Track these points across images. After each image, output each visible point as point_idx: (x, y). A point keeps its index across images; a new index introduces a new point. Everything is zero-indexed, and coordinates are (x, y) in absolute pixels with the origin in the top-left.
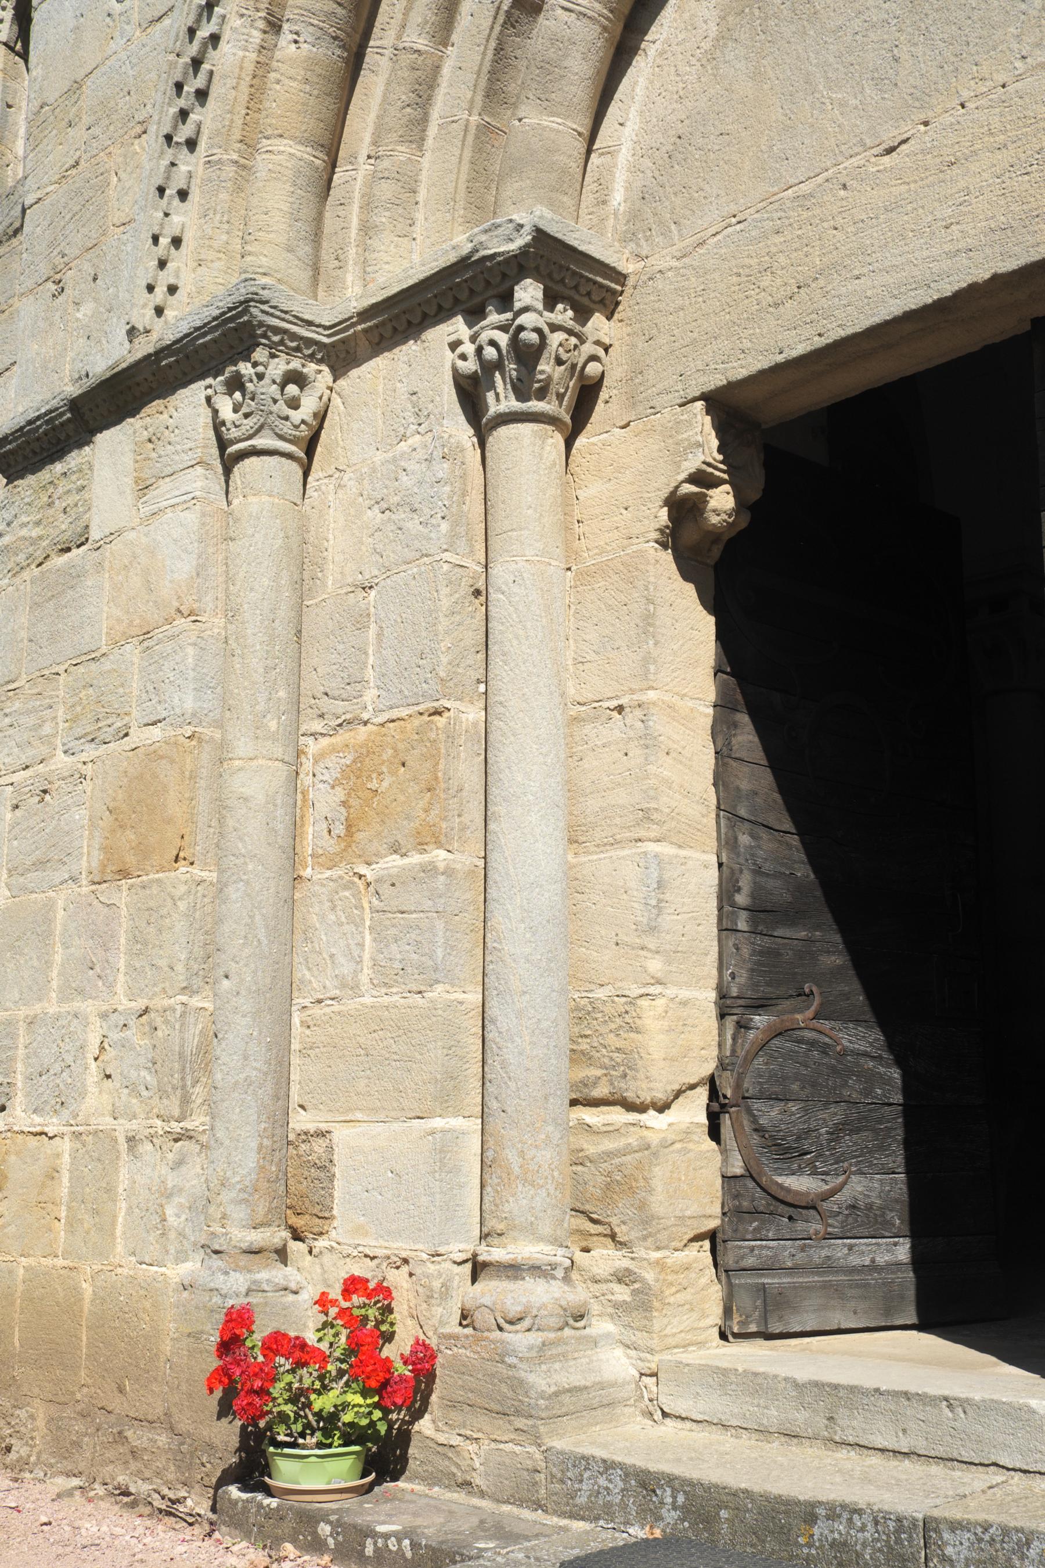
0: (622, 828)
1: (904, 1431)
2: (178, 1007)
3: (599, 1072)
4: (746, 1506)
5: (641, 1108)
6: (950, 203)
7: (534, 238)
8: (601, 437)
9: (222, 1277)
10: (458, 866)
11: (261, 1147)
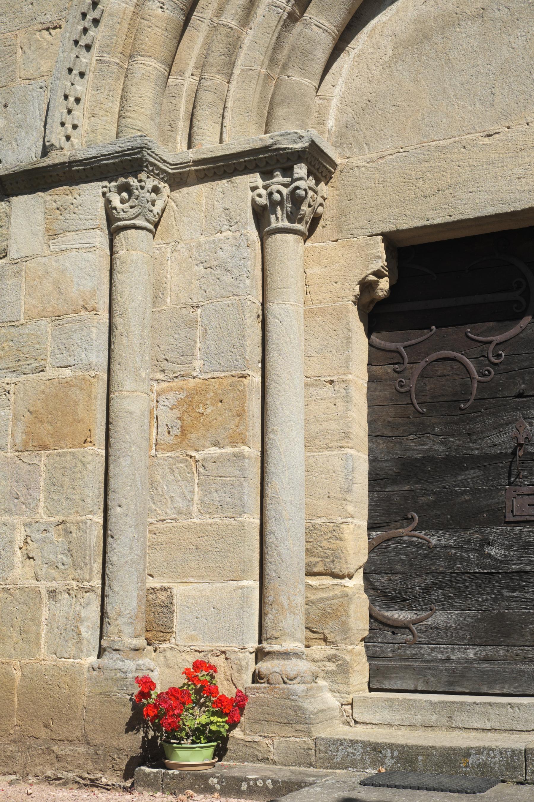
0: (332, 441)
1: (488, 720)
2: (88, 521)
3: (317, 560)
4: (432, 753)
5: (342, 577)
6: (521, 168)
7: (310, 145)
8: (320, 244)
9: (121, 663)
10: (252, 455)
11: (138, 595)
